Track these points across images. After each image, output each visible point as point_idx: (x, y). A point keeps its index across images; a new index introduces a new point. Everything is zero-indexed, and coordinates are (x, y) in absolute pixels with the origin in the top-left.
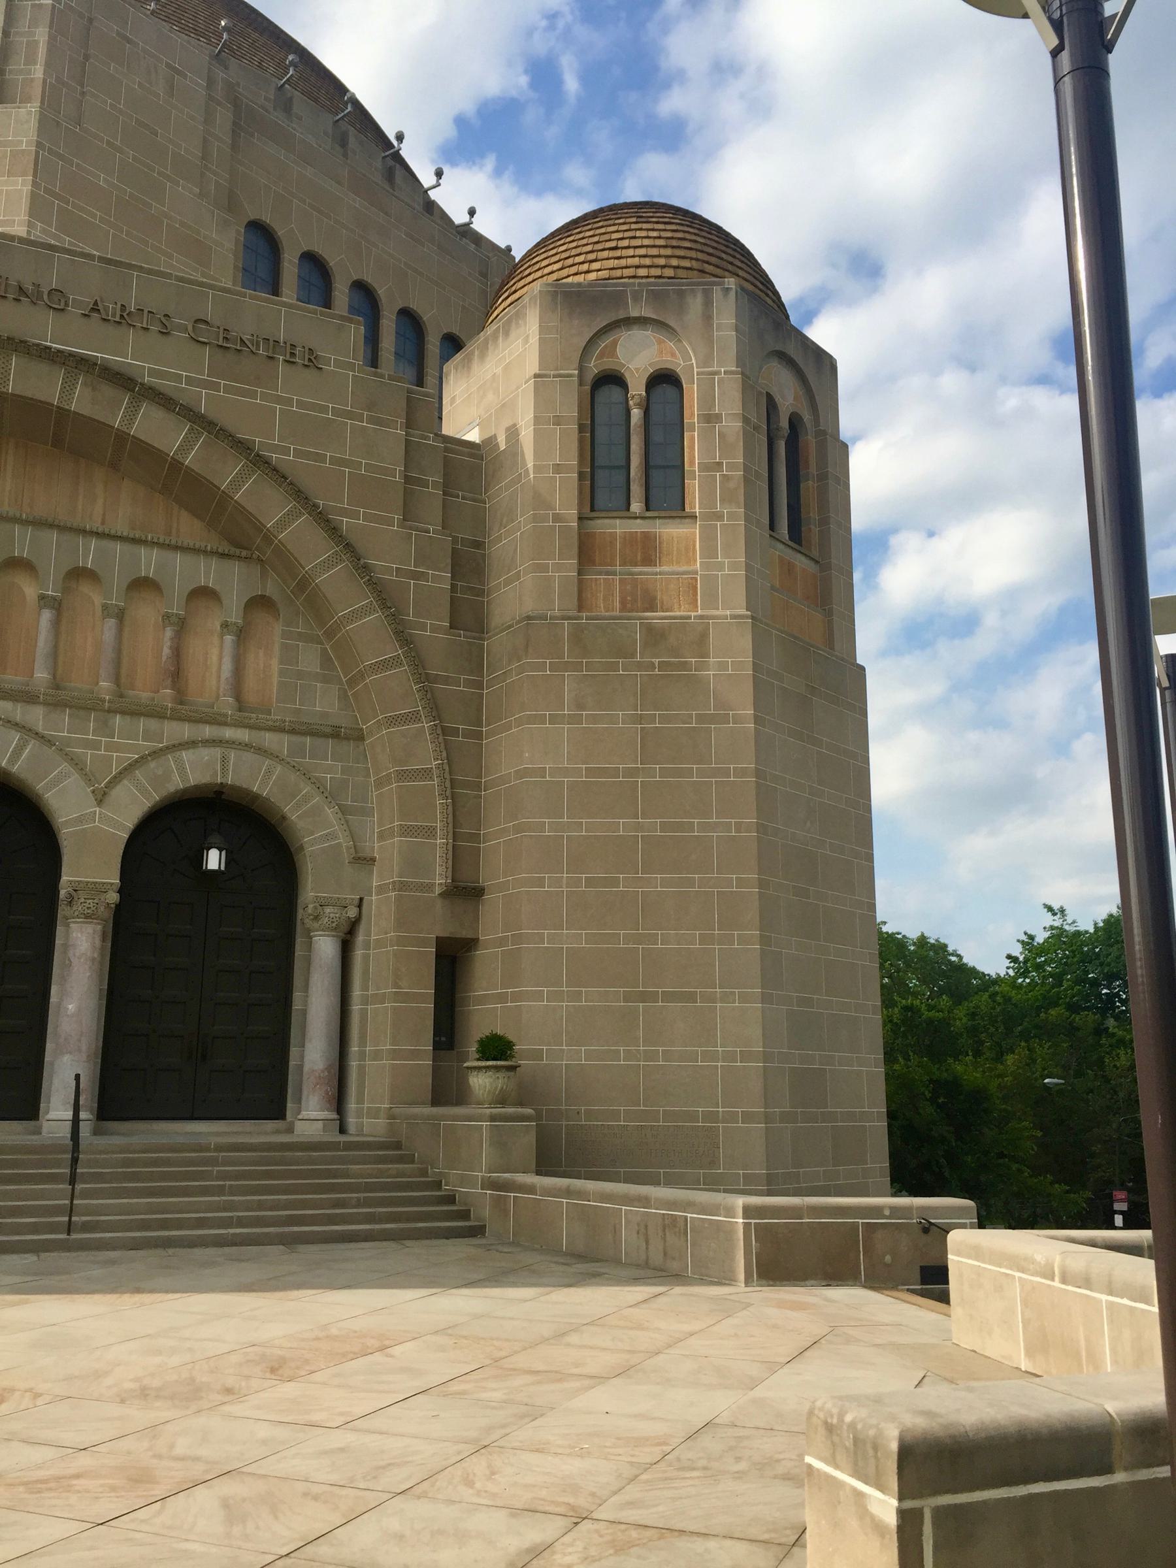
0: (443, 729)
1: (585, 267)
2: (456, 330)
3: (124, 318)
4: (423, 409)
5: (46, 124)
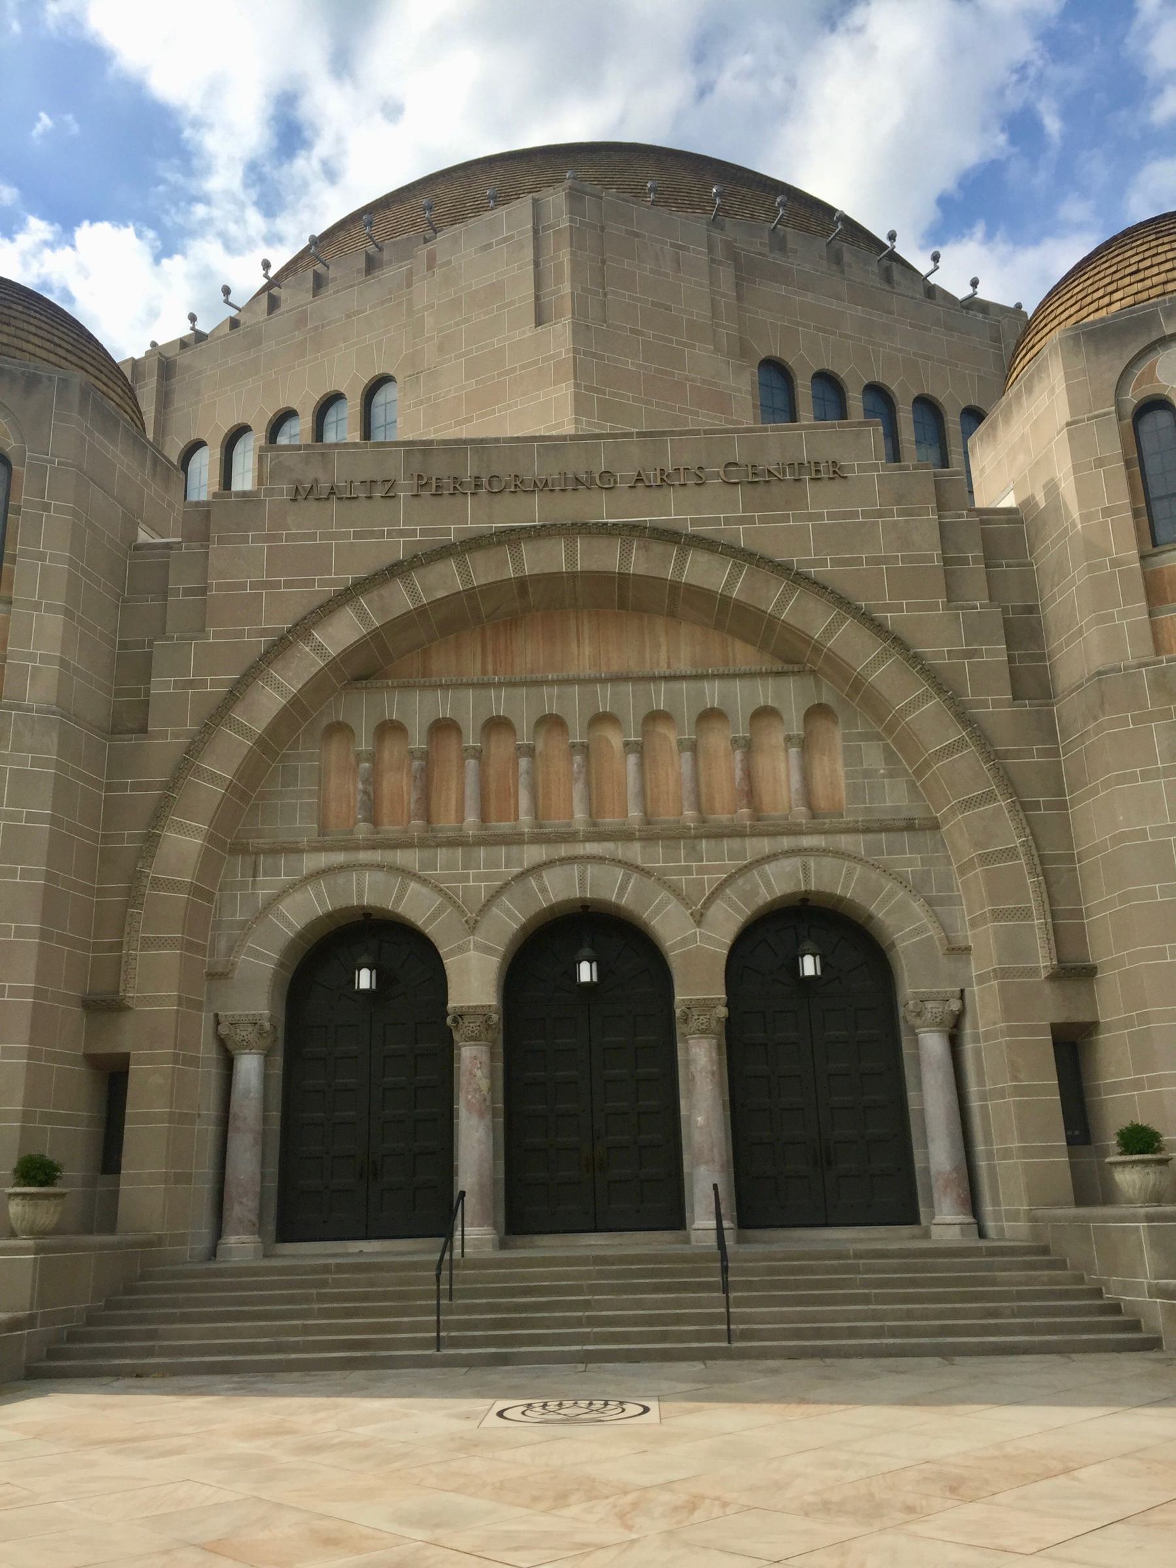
0: (1022, 803)
1: (1106, 300)
2: (974, 402)
3: (665, 481)
4: (951, 486)
5: (579, 330)
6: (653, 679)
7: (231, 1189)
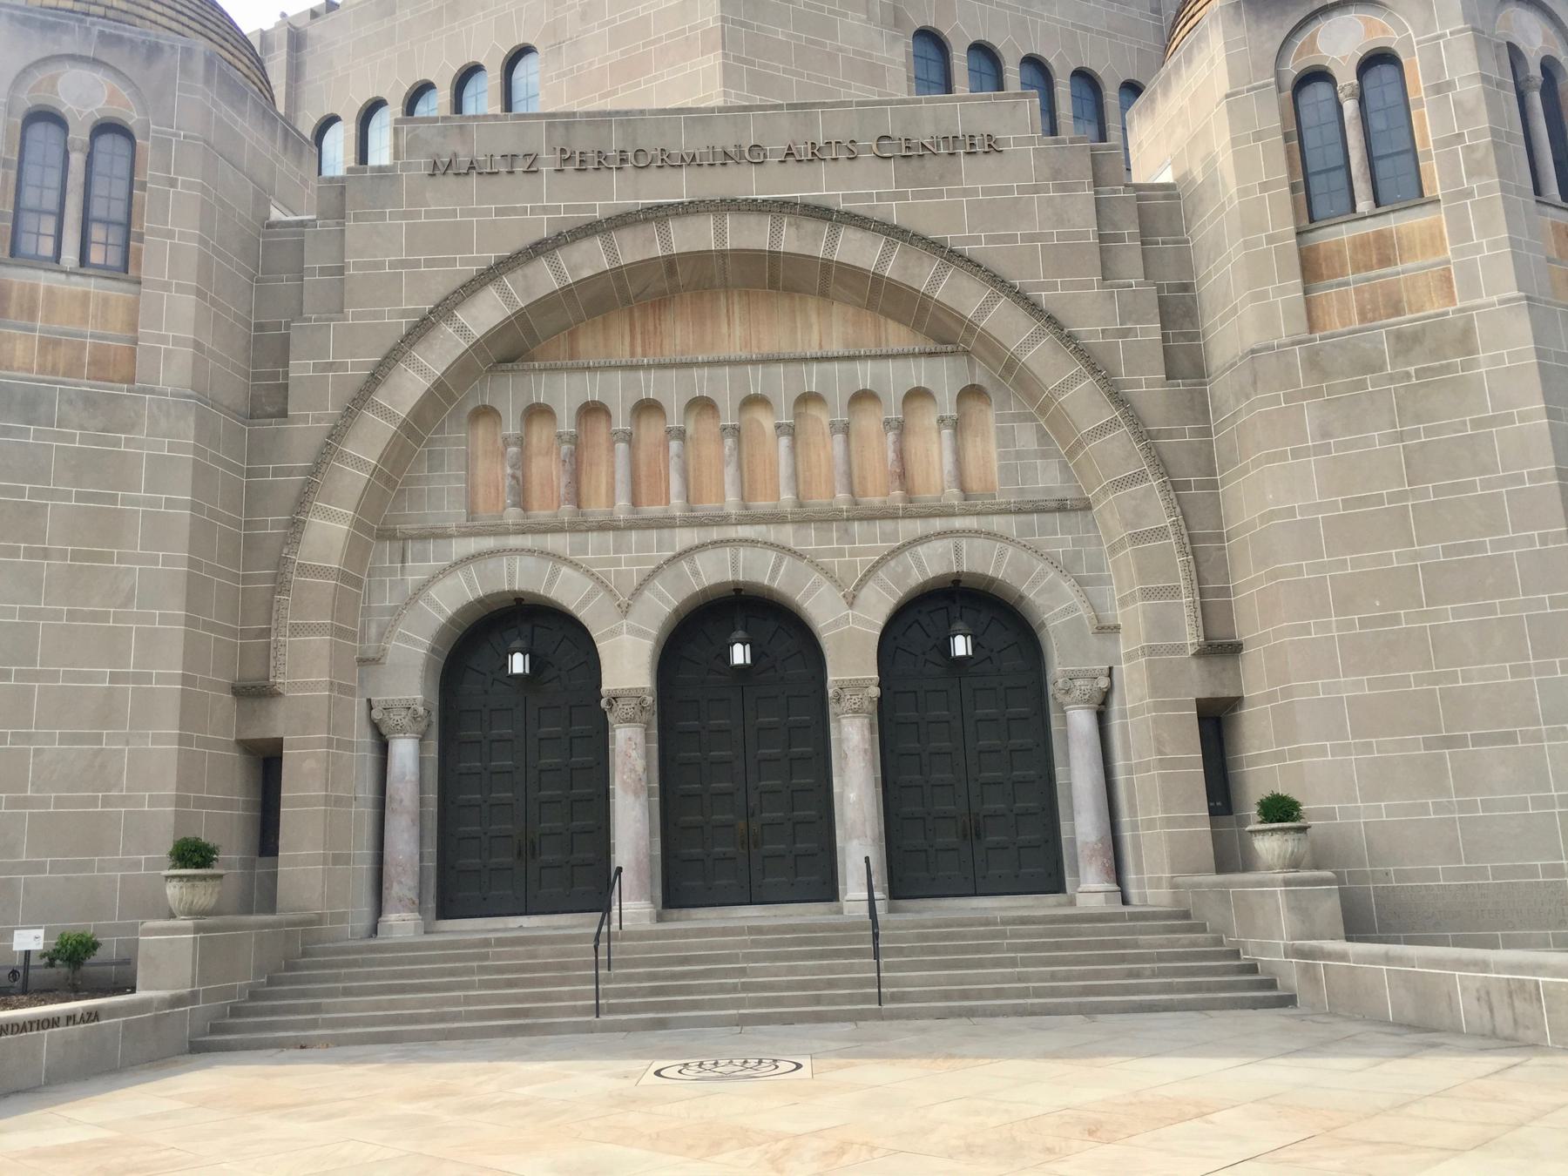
3: (816, 155)
6: (805, 360)
7: (390, 869)
